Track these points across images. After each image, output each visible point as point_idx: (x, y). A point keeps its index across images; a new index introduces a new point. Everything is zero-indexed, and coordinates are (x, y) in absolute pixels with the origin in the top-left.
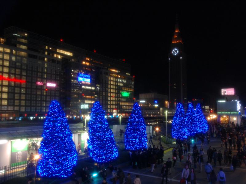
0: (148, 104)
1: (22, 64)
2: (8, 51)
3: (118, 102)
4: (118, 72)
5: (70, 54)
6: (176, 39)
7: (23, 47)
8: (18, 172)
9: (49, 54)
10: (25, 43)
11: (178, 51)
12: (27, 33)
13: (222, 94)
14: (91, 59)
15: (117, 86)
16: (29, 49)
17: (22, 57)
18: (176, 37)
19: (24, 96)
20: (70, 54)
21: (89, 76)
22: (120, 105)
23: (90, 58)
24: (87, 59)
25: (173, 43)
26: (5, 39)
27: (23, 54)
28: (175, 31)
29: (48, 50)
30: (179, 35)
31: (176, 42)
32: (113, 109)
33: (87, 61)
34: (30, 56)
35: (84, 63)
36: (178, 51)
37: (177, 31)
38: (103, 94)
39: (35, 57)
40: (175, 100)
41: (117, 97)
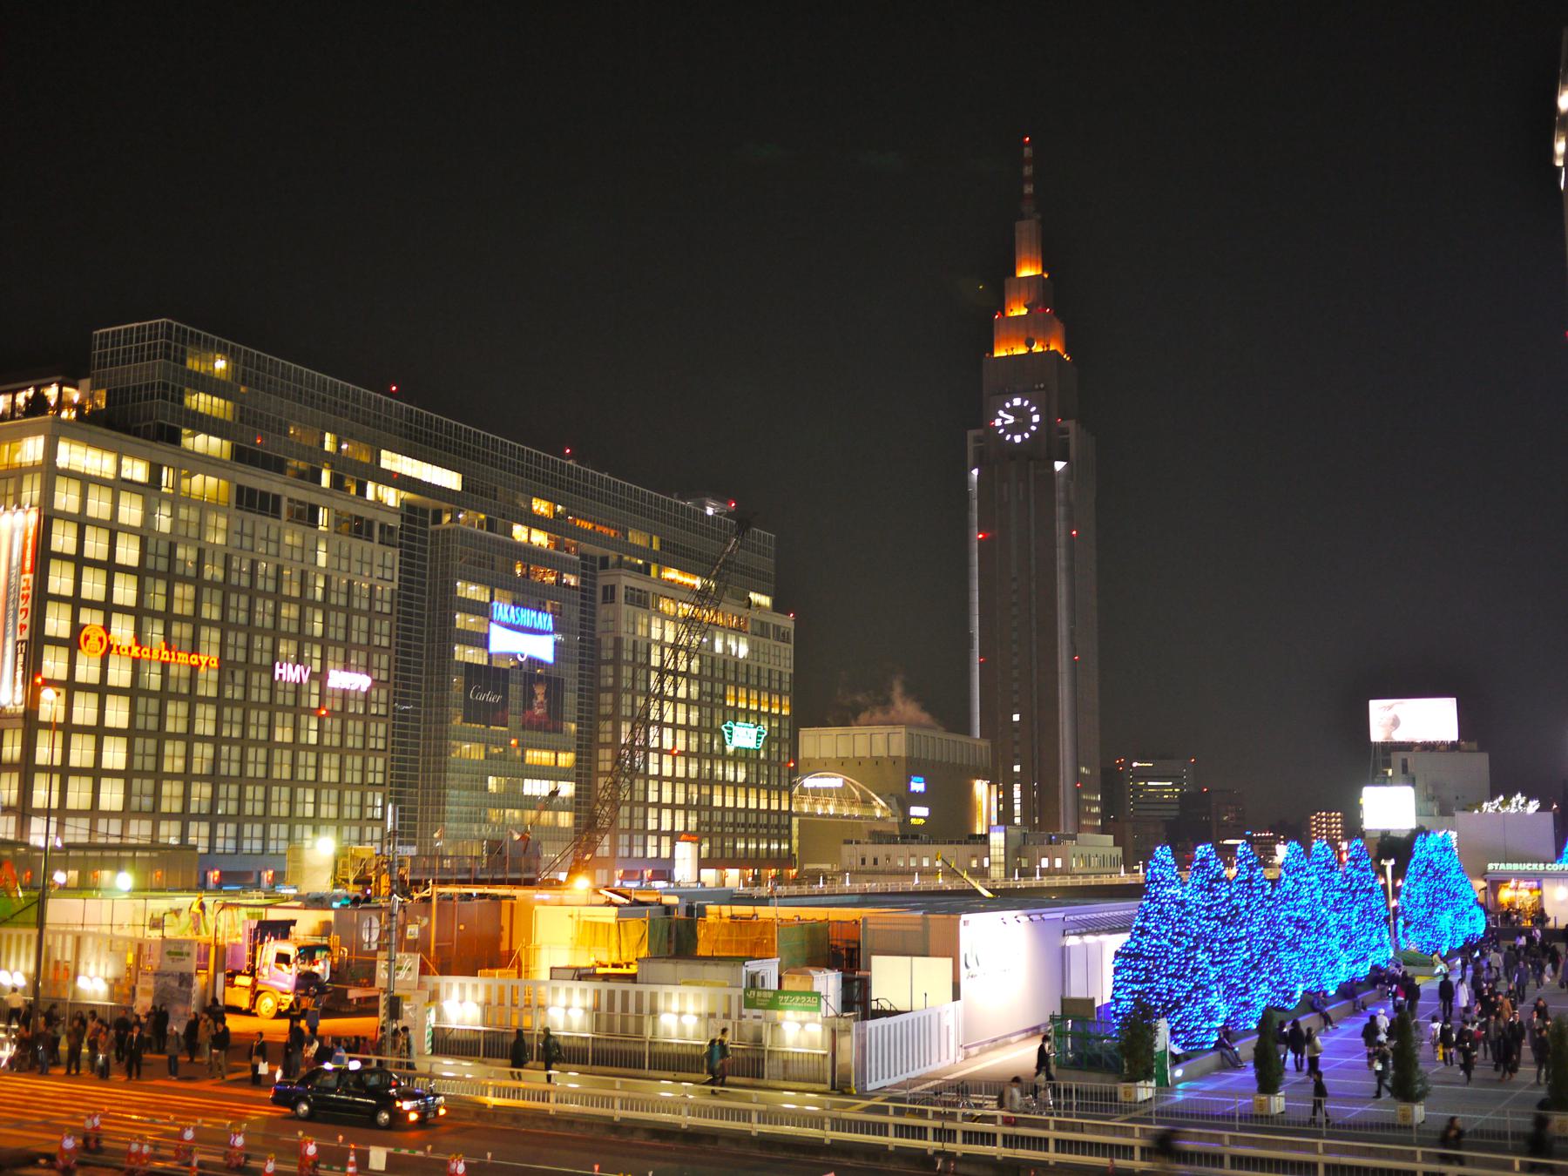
0: (866, 802)
1: (201, 553)
2: (137, 470)
3: (705, 791)
4: (705, 589)
5: (450, 480)
6: (1025, 330)
7: (204, 443)
8: (642, 721)
9: (337, 482)
10: (215, 420)
11: (1036, 418)
12: (231, 355)
13: (1377, 735)
14: (559, 508)
15: (704, 653)
16: (241, 455)
17: (204, 506)
18: (1024, 311)
19: (119, 785)
20: (450, 480)
21: (545, 620)
22: (711, 807)
23: (554, 501)
24: (541, 507)
25: (1000, 353)
26: (907, 709)
27: (202, 485)
28: (1013, 273)
29: (336, 461)
30: (1042, 293)
31: (1021, 350)
32: (674, 836)
33: (534, 522)
34: (246, 499)
35: (519, 533)
36: (1018, 439)
37: (1026, 272)
38: (617, 733)
39: (266, 504)
40: (1017, 768)
41: (699, 756)
